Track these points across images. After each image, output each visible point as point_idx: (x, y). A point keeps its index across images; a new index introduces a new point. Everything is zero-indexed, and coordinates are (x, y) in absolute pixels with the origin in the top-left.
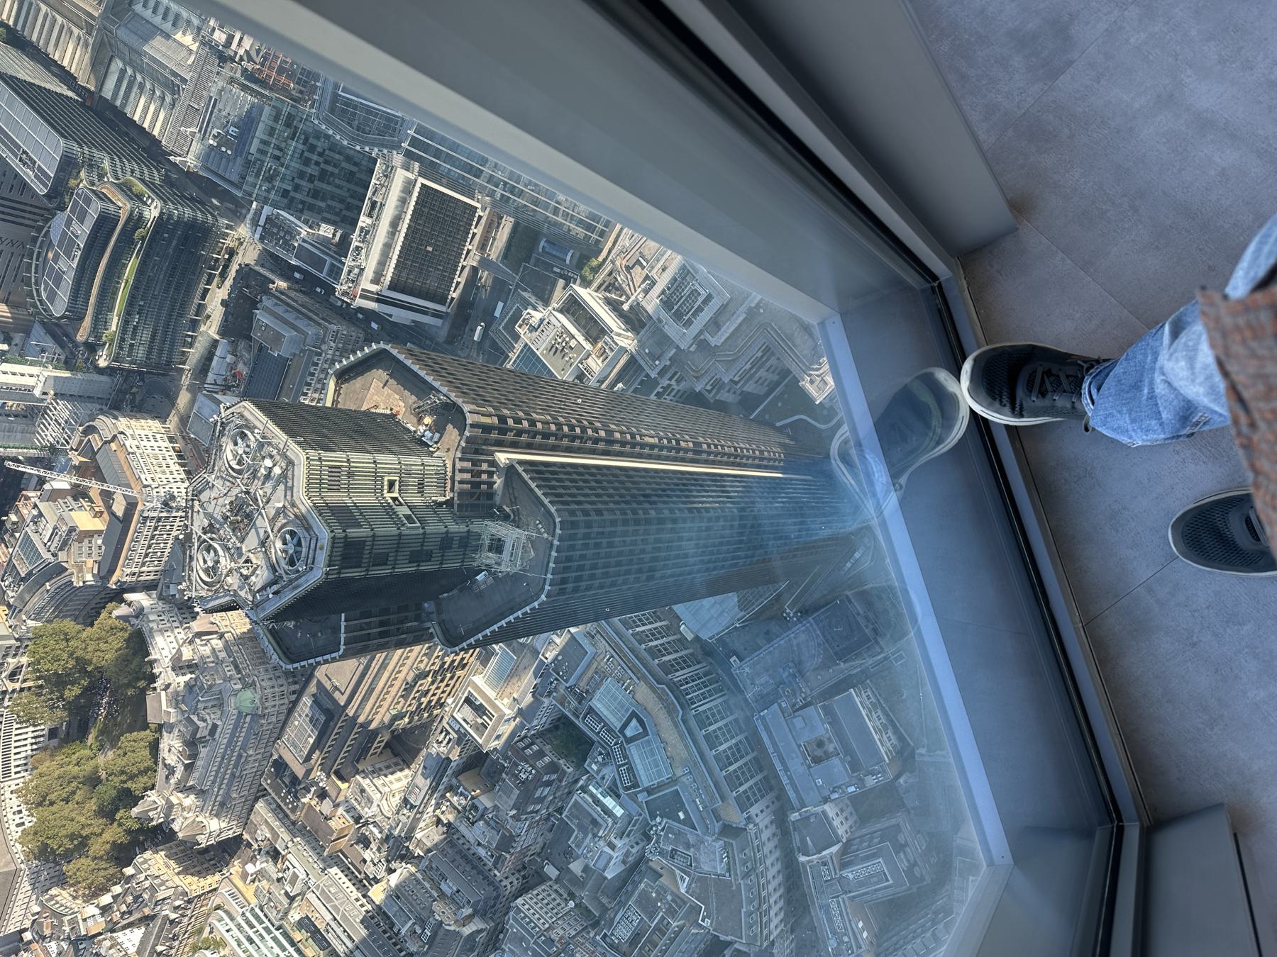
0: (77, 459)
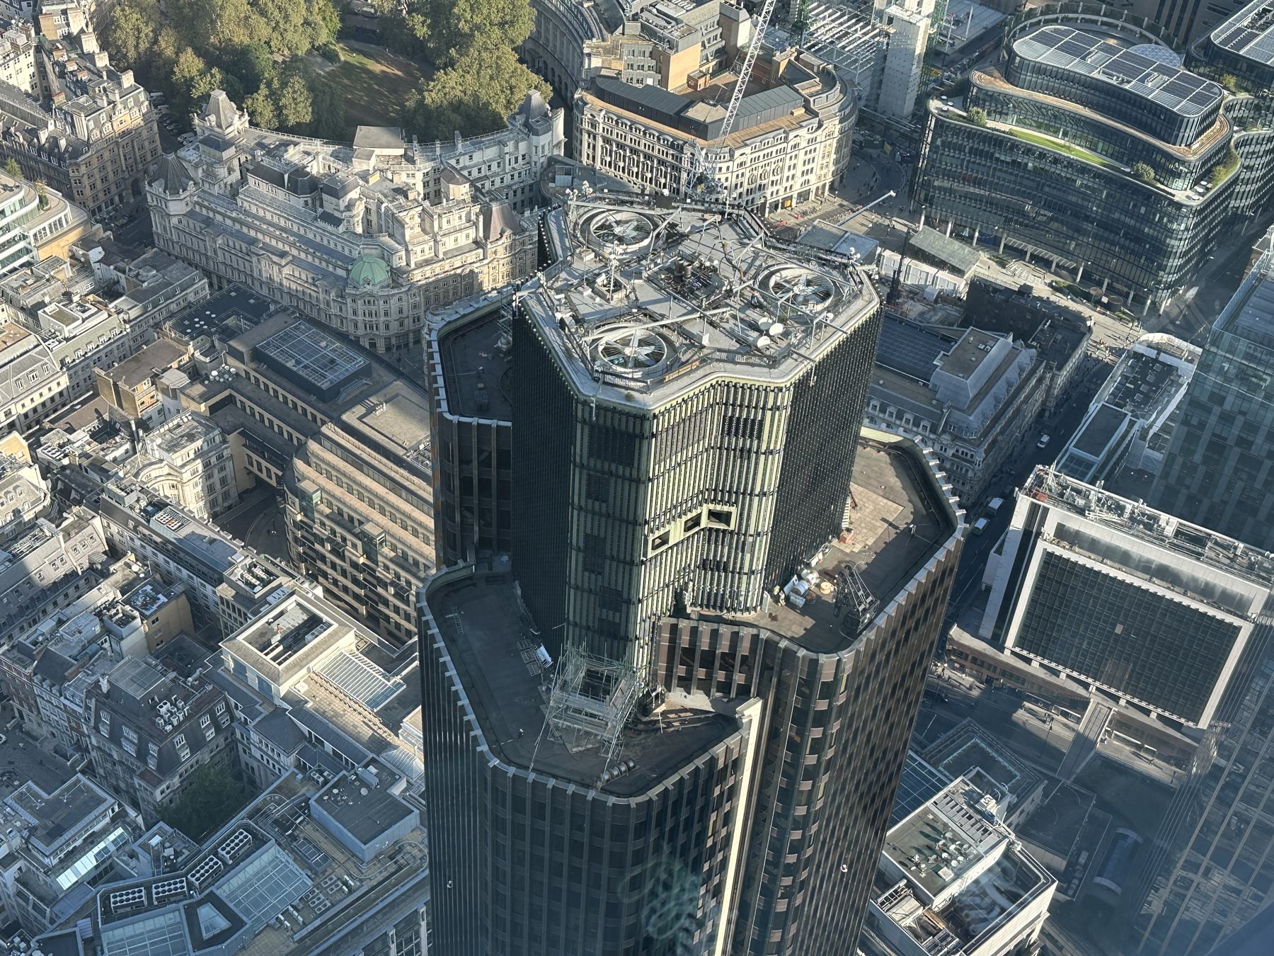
0: (783, 59)
